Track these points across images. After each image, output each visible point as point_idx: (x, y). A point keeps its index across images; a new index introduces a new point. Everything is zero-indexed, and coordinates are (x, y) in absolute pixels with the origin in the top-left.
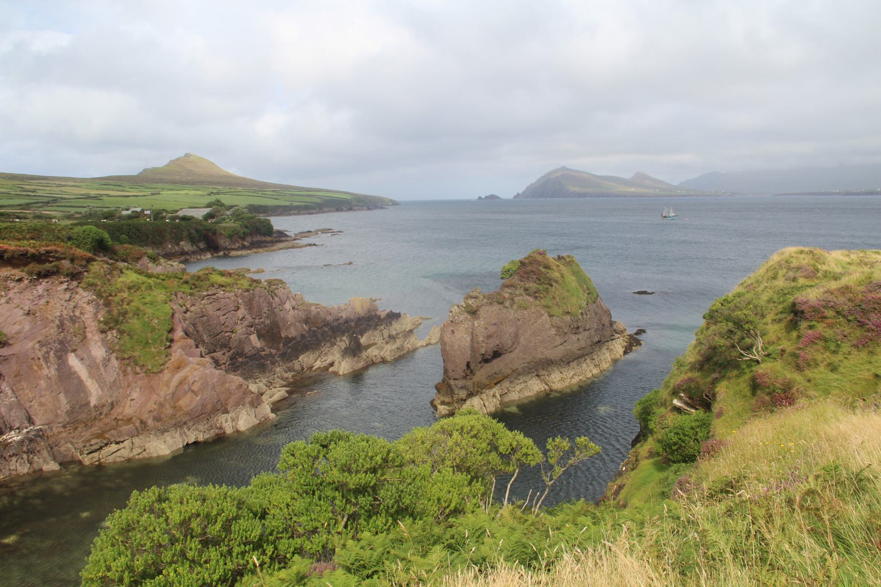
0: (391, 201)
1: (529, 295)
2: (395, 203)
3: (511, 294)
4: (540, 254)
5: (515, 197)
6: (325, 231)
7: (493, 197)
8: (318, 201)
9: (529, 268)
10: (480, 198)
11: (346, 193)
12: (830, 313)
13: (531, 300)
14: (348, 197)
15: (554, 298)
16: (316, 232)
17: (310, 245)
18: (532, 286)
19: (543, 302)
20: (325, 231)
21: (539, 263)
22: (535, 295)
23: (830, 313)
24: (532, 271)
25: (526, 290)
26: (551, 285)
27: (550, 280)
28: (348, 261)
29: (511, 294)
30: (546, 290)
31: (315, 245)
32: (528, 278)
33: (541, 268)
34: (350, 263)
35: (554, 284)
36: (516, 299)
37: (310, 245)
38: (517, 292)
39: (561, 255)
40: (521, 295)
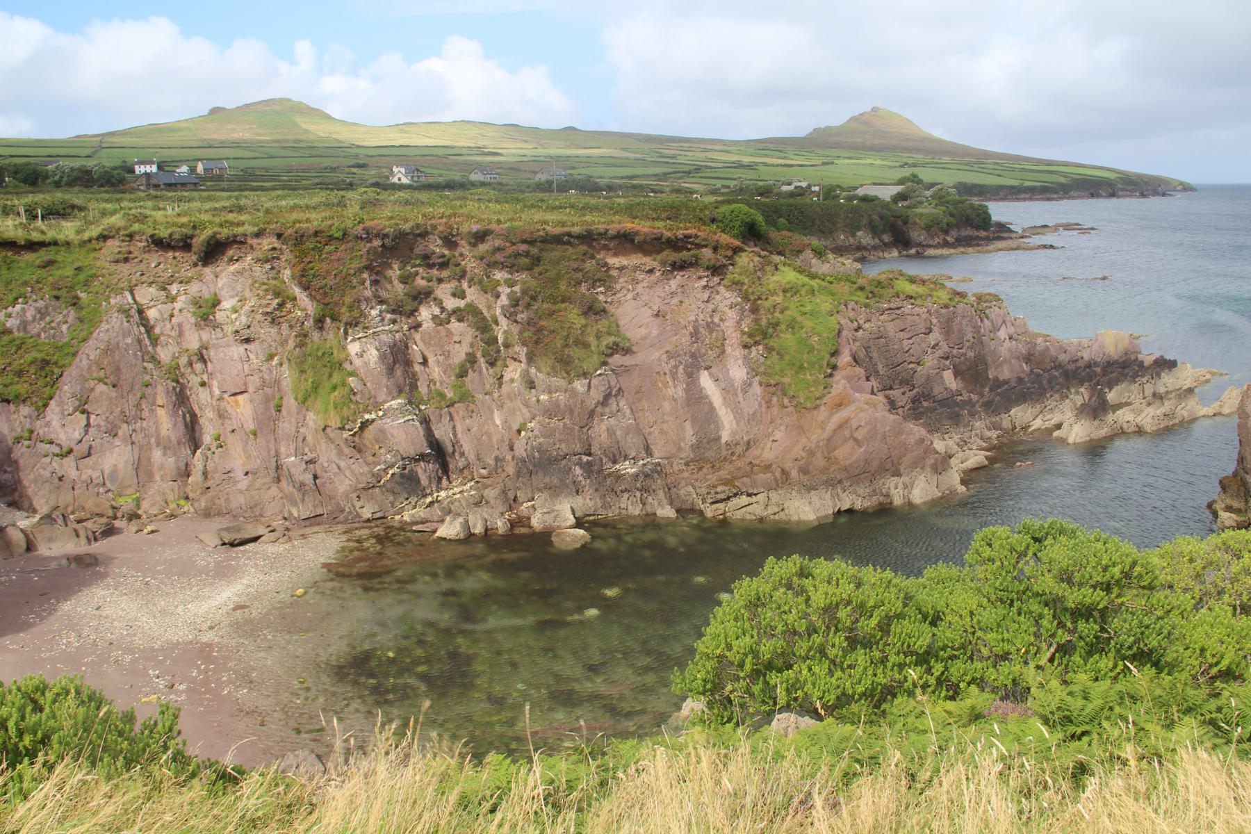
0: (1181, 183)
2: (1187, 188)
6: (1068, 227)
8: (1062, 180)
14: (1112, 176)
17: (1045, 247)
20: (1068, 227)
31: (1051, 247)
34: (1104, 278)
37: (1045, 247)
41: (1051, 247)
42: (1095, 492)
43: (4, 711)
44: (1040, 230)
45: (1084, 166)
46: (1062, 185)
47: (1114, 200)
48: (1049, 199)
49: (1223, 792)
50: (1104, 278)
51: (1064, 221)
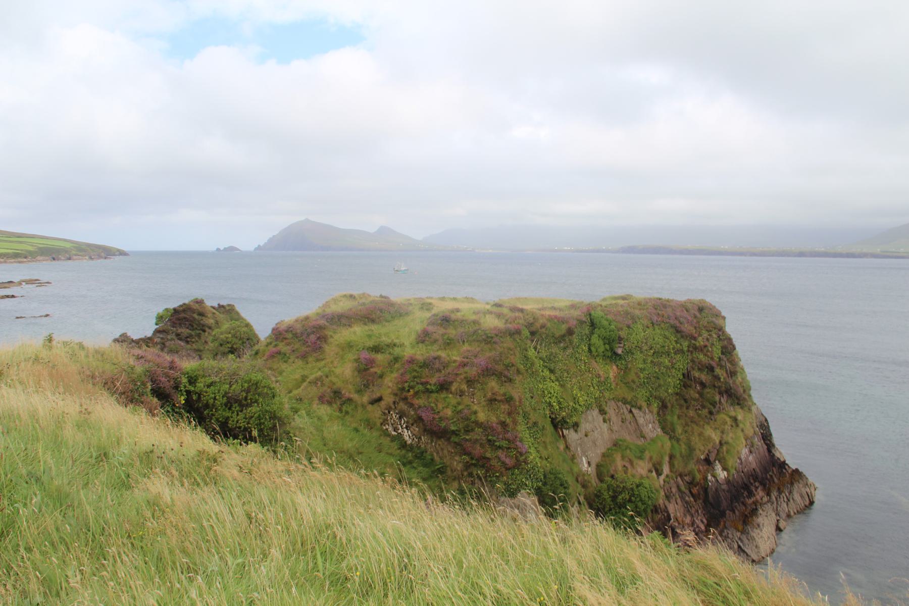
0: (118, 250)
1: (180, 339)
2: (122, 253)
3: (162, 338)
4: (197, 302)
5: (256, 249)
6: (29, 282)
7: (232, 249)
8: (30, 248)
9: (183, 315)
10: (218, 249)
11: (65, 240)
12: (290, 336)
13: (182, 344)
14: (68, 245)
15: (206, 342)
16: (20, 283)
17: (8, 297)
18: (185, 331)
19: (195, 346)
20: (29, 282)
21: (193, 311)
22: (187, 340)
23: (290, 336)
24: (185, 318)
25: (178, 335)
26: (204, 331)
27: (203, 326)
28: (44, 314)
29: (162, 338)
30: (199, 336)
31: (13, 296)
32: (180, 324)
33: (195, 316)
34: (47, 315)
35: (207, 329)
36: (167, 344)
37: (8, 297)
38: (169, 337)
39: (222, 304)
40: (172, 340)
41: (13, 296)
42: (203, 380)
43: (152, 601)
44: (7, 285)
45: (47, 238)
46: (30, 253)
47: (70, 262)
48: (20, 262)
49: (142, 563)
50: (47, 315)
51: (28, 278)
